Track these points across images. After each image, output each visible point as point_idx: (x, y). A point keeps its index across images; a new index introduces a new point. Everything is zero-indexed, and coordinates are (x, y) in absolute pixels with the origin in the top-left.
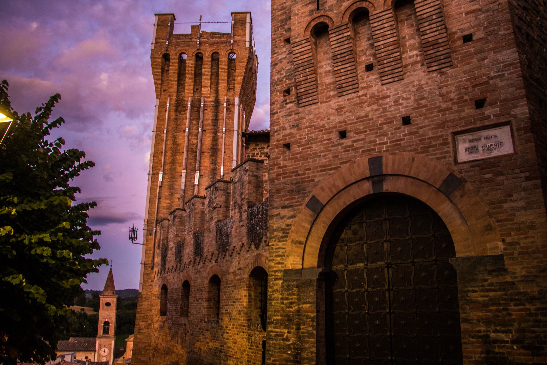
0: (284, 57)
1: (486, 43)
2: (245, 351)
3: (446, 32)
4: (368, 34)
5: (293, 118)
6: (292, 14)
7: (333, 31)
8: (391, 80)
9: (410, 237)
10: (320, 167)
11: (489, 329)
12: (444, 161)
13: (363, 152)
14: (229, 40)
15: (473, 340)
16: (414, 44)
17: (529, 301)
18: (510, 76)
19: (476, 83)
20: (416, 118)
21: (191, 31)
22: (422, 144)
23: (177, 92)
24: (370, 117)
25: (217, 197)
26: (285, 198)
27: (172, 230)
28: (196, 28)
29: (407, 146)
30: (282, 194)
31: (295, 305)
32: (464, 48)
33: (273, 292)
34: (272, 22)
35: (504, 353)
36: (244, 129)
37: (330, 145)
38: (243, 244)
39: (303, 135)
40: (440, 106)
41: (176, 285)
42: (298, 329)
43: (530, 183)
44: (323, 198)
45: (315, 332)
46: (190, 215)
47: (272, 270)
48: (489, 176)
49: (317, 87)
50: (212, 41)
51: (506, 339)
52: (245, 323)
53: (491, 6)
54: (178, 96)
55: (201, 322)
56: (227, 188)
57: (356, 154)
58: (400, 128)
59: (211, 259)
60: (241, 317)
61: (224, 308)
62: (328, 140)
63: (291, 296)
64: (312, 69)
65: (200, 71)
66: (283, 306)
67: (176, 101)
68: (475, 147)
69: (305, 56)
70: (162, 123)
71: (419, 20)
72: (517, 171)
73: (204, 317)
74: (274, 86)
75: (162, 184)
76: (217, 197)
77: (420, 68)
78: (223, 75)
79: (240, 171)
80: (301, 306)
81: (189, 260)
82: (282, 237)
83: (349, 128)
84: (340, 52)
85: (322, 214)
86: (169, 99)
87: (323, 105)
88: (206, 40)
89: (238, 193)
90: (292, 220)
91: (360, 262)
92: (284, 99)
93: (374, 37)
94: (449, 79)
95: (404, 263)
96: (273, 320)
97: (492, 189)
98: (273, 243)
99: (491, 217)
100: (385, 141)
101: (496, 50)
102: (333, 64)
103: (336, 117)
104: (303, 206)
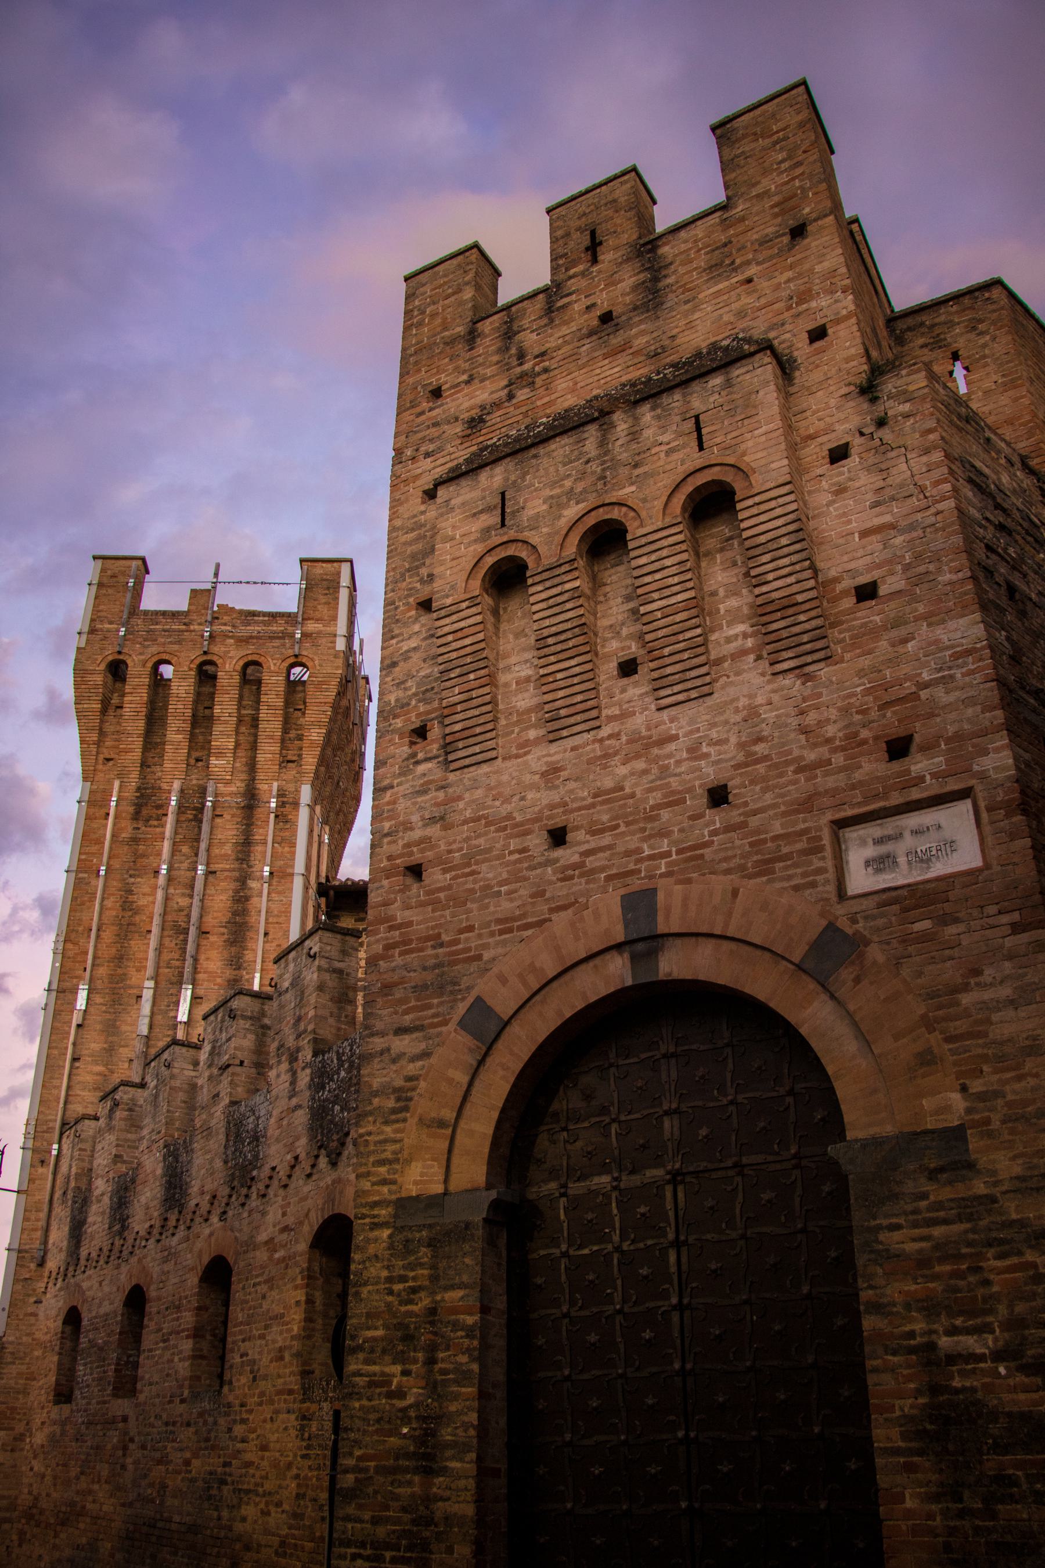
0: (415, 645)
1: (909, 603)
2: (289, 1466)
3: (815, 576)
4: (627, 587)
5: (431, 799)
6: (438, 537)
7: (537, 579)
8: (680, 697)
9: (730, 1098)
10: (499, 921)
11: (935, 1326)
12: (811, 894)
13: (609, 878)
14: (290, 629)
15: (896, 1359)
16: (739, 608)
17: (1033, 1242)
18: (967, 679)
19: (887, 698)
20: (743, 790)
21: (190, 604)
22: (756, 853)
23: (141, 766)
24: (628, 790)
25: (233, 1036)
26: (404, 1007)
27: (105, 1143)
28: (201, 597)
29: (720, 861)
30: (398, 996)
31: (422, 1294)
32: (859, 614)
33: (364, 1262)
34: (388, 559)
35: (973, 1390)
36: (323, 874)
37: (526, 865)
38: (296, 1158)
39: (455, 841)
40: (801, 758)
41: (106, 1303)
42: (431, 1361)
43: (1024, 938)
44: (504, 1003)
45: (475, 1367)
46: (156, 1096)
47: (363, 1201)
48: (925, 925)
49: (495, 720)
50: (244, 631)
51: (980, 1350)
52: (294, 1382)
53: (919, 516)
54: (143, 776)
55: (170, 1402)
56: (263, 1014)
57: (592, 886)
58: (701, 816)
59: (209, 1212)
60: (285, 1367)
61: (239, 1350)
62: (520, 852)
63: (412, 1270)
64: (482, 672)
65: (207, 712)
66: (390, 1298)
67: (138, 789)
68: (888, 857)
69: (467, 641)
70: (94, 848)
71: (747, 549)
72: (992, 909)
73: (181, 1387)
74: (386, 719)
75: (84, 1019)
76: (233, 1036)
77: (751, 666)
78: (271, 725)
79: (295, 960)
80: (438, 1298)
81: (147, 1225)
82: (394, 1111)
83: (575, 819)
84: (554, 630)
85: (500, 1045)
86: (117, 784)
87: (508, 764)
88: (229, 628)
89: (290, 1020)
90: (421, 1063)
91: (600, 1174)
92: (410, 751)
93: (640, 591)
94: (824, 691)
95: (714, 1170)
96: (364, 1342)
97: (933, 958)
98: (370, 1128)
99: (931, 1030)
100: (666, 849)
101: (934, 619)
102: (536, 662)
103: (542, 792)
104: (452, 1026)
